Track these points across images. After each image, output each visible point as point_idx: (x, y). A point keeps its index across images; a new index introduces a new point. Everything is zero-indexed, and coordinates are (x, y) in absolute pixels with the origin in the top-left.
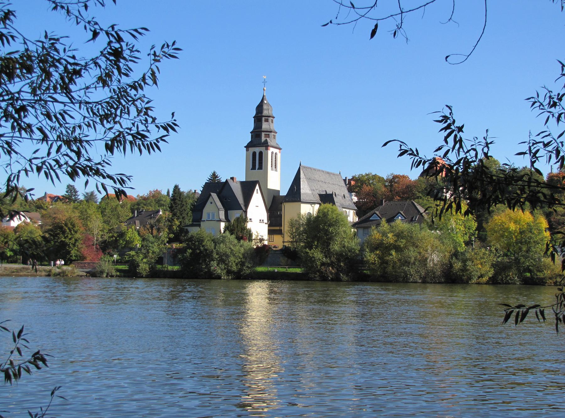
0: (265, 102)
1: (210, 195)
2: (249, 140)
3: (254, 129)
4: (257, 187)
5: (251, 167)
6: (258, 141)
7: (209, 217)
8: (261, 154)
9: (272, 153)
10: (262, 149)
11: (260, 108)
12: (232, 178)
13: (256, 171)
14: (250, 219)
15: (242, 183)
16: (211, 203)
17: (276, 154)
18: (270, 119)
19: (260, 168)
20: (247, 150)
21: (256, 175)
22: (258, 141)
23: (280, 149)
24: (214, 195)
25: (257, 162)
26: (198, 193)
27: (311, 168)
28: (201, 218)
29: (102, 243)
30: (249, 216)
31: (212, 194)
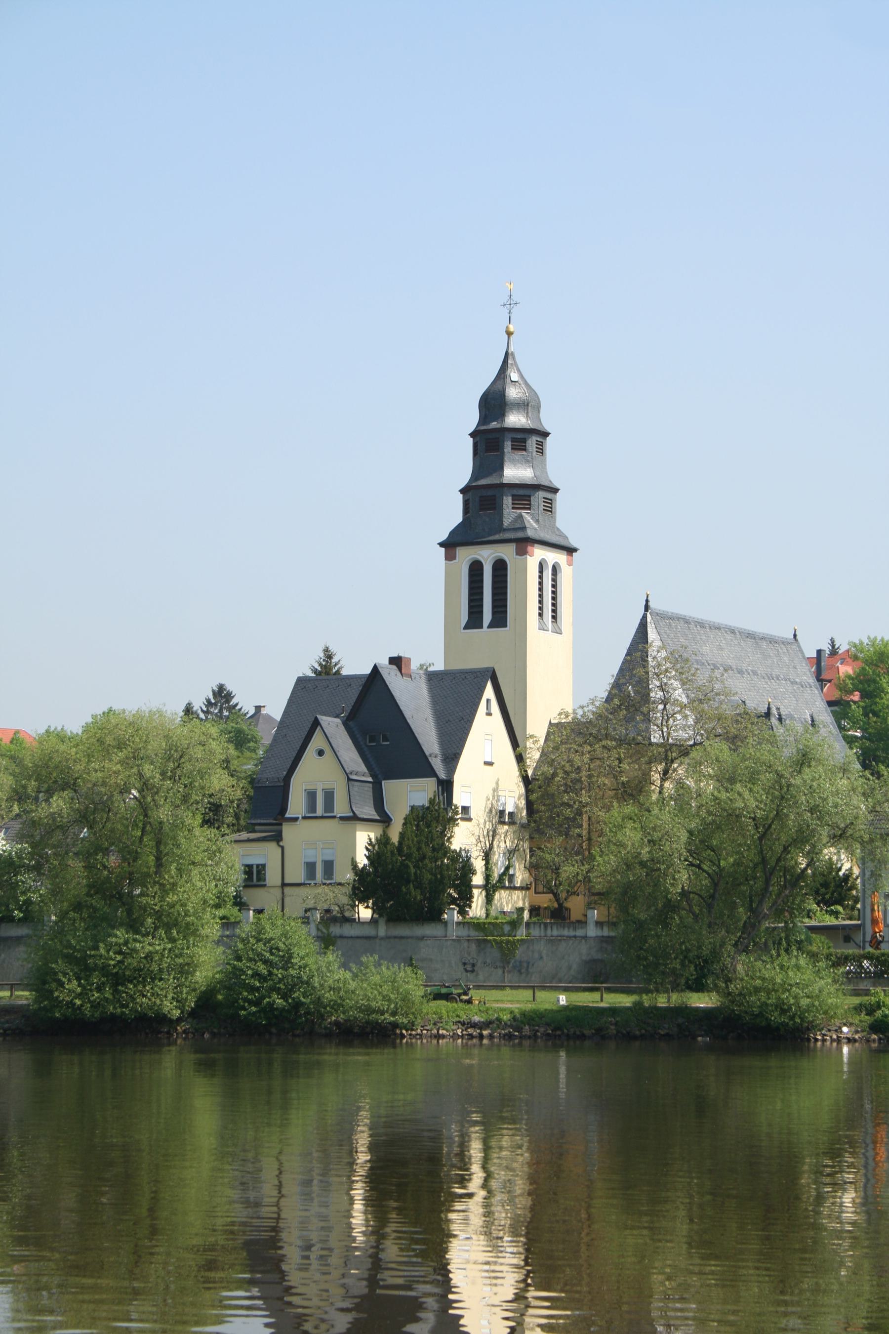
0: (514, 376)
1: (316, 723)
2: (456, 516)
3: (475, 475)
4: (489, 692)
5: (464, 618)
6: (498, 511)
7: (312, 806)
8: (500, 567)
9: (541, 567)
10: (507, 552)
11: (493, 403)
12: (397, 661)
13: (485, 633)
14: (466, 809)
15: (433, 678)
16: (321, 753)
17: (555, 570)
18: (532, 442)
19: (500, 619)
20: (450, 557)
21: (483, 648)
22: (498, 511)
23: (571, 551)
24: (332, 725)
25: (487, 601)
26: (269, 718)
27: (686, 621)
28: (284, 809)
29: (218, 983)
30: (459, 798)
31: (324, 720)
